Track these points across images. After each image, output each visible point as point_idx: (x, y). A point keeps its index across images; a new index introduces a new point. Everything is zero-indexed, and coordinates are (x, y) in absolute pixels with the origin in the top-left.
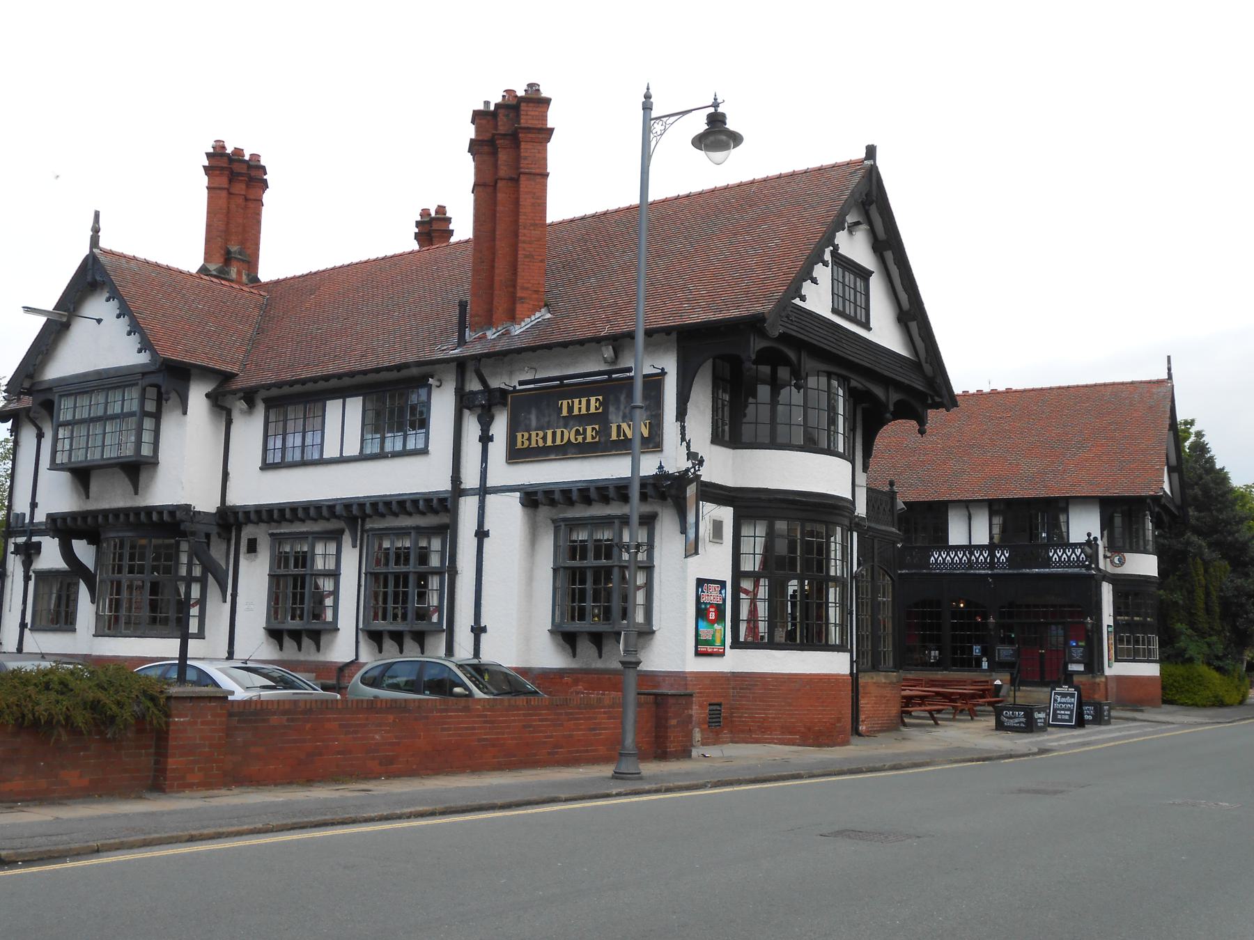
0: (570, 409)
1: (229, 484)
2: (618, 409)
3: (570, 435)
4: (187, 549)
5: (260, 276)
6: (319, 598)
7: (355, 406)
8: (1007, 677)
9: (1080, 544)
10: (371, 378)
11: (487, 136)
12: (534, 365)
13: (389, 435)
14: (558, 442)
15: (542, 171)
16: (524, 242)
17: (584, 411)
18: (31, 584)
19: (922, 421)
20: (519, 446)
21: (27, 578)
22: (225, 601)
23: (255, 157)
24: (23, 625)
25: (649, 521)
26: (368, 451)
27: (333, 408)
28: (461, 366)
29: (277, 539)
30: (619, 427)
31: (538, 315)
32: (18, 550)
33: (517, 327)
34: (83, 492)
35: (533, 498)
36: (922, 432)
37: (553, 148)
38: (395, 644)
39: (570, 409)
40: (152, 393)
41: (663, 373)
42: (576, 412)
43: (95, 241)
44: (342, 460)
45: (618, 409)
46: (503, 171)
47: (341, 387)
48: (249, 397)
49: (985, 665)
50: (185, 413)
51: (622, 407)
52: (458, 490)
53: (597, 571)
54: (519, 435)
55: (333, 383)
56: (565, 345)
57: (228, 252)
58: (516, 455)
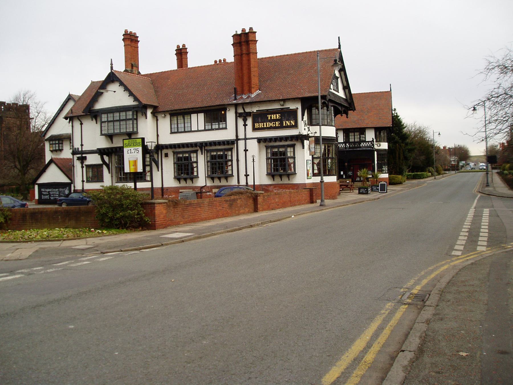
0: (271, 117)
1: (74, 128)
2: (285, 118)
3: (271, 124)
4: (149, 157)
5: (140, 70)
6: (193, 169)
7: (201, 116)
8: (351, 180)
9: (371, 141)
10: (205, 109)
11: (238, 41)
12: (259, 105)
13: (214, 124)
14: (268, 126)
15: (256, 52)
16: (253, 72)
17: (275, 118)
18: (84, 169)
19: (347, 114)
20: (256, 127)
21: (82, 167)
22: (158, 171)
23: (135, 33)
24: (83, 181)
25: (293, 146)
26: (207, 128)
27: (194, 116)
28: (236, 106)
29: (174, 153)
30: (286, 122)
31: (257, 91)
32: (78, 159)
33: (252, 95)
34: (110, 140)
35: (260, 140)
36: (347, 117)
37: (258, 44)
38: (191, 181)
39: (271, 117)
40: (135, 113)
41: (297, 109)
42: (273, 118)
43: (112, 68)
44: (198, 131)
45: (285, 118)
46: (244, 52)
47: (197, 111)
48: (164, 112)
49: (344, 177)
50: (146, 118)
51: (286, 117)
52: (237, 139)
53: (281, 159)
54: (256, 124)
55: (195, 110)
56: (269, 101)
57: (132, 65)
58: (254, 129)
